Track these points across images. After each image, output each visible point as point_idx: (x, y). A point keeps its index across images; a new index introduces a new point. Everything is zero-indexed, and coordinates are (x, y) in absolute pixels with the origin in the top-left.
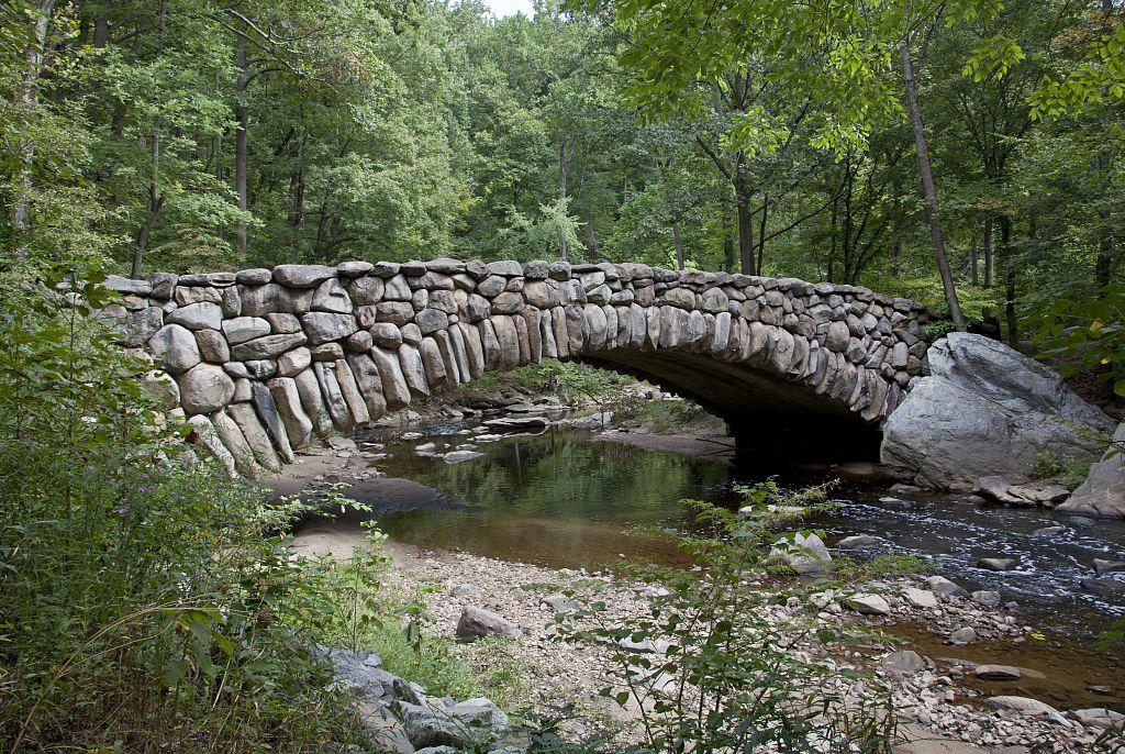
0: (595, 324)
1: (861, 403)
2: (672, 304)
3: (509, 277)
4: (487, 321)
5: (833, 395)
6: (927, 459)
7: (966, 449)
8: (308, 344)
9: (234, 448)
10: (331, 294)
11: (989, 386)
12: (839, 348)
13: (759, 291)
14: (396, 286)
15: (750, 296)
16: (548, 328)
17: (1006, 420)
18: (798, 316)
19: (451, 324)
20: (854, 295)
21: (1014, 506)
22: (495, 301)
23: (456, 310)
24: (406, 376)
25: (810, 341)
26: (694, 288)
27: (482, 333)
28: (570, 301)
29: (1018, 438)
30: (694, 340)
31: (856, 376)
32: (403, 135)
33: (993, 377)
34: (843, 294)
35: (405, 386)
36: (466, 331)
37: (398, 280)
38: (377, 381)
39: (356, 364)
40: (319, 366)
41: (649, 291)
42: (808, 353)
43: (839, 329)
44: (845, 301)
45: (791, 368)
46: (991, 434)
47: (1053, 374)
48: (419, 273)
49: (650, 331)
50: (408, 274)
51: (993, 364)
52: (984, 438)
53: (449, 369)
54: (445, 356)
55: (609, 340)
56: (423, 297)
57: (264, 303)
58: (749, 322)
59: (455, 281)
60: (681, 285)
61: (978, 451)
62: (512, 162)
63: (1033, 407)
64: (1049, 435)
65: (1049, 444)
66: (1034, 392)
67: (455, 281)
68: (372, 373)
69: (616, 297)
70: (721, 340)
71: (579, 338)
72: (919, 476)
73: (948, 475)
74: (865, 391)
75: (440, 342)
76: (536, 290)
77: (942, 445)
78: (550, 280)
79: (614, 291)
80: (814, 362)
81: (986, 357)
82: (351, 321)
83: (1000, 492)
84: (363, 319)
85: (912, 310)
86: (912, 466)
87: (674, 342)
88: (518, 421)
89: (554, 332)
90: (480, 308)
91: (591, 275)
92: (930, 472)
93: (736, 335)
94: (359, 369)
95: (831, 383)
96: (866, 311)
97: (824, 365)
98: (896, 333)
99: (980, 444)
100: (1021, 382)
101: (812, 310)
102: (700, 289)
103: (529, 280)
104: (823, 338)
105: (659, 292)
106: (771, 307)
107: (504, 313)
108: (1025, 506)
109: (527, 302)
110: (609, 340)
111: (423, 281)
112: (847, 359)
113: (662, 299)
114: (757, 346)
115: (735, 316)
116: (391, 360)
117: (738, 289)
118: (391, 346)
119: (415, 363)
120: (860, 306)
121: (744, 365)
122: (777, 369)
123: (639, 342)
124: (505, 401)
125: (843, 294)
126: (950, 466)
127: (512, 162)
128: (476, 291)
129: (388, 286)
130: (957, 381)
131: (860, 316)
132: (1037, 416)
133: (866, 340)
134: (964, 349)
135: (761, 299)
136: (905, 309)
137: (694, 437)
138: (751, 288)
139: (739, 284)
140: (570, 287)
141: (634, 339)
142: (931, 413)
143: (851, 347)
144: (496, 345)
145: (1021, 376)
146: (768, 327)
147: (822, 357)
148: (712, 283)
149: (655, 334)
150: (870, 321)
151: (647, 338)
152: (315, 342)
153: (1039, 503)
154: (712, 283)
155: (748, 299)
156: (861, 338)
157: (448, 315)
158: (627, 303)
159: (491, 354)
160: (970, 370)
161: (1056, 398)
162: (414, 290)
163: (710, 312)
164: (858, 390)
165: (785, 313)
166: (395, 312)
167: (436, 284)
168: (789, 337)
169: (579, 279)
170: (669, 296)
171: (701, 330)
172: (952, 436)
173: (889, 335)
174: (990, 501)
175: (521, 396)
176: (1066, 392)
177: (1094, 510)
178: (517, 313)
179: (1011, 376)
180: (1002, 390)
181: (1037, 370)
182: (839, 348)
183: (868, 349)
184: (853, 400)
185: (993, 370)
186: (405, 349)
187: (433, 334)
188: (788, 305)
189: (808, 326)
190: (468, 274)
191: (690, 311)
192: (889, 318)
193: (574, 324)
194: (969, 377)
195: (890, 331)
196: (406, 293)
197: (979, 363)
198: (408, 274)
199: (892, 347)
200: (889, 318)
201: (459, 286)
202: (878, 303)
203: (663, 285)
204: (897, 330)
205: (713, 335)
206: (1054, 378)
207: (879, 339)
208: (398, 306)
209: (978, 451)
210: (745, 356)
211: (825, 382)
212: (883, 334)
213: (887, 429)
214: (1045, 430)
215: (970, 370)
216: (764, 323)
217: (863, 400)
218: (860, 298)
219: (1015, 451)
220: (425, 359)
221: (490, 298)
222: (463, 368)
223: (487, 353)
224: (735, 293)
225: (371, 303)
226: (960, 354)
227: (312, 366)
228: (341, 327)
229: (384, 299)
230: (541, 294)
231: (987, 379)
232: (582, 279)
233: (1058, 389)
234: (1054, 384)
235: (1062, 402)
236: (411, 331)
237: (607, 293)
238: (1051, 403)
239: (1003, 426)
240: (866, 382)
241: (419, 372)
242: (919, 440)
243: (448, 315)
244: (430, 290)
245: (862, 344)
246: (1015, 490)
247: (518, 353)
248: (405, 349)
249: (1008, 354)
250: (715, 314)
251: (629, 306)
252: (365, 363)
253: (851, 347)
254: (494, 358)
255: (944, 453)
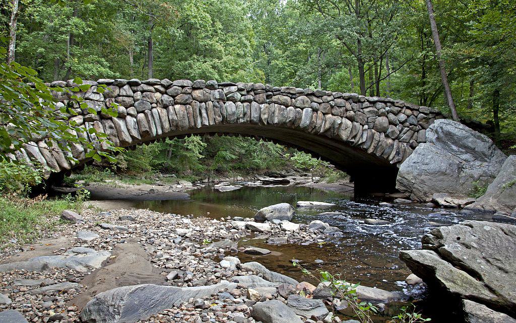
0: (229, 109)
1: (395, 160)
2: (275, 103)
3: (183, 87)
4: (170, 107)
6: (415, 185)
8: (82, 114)
10: (93, 93)
11: (454, 147)
12: (383, 130)
13: (329, 98)
14: (125, 90)
15: (324, 101)
16: (203, 111)
17: (458, 165)
18: (355, 112)
19: (152, 108)
20: (393, 103)
21: (446, 207)
22: (176, 98)
23: (155, 101)
24: (128, 130)
26: (291, 96)
27: (168, 112)
28: (216, 99)
29: (464, 175)
30: (288, 121)
31: (392, 145)
32: (219, 47)
33: (456, 142)
34: (385, 103)
36: (160, 111)
37: (126, 87)
38: (114, 131)
39: (104, 124)
40: (86, 123)
41: (262, 96)
43: (382, 120)
44: (387, 106)
47: (487, 140)
48: (137, 84)
49: (262, 115)
50: (131, 84)
52: (444, 174)
53: (150, 128)
54: (148, 122)
55: (238, 119)
56: (138, 95)
57: (62, 95)
58: (324, 114)
59: (155, 88)
60: (282, 93)
62: (290, 63)
63: (476, 159)
64: (481, 173)
67: (155, 88)
69: (243, 98)
70: (305, 121)
71: (219, 116)
72: (412, 195)
73: (425, 194)
74: (398, 153)
75: (146, 115)
76: (197, 93)
77: (423, 177)
78: (205, 89)
79: (242, 95)
80: (365, 136)
82: (102, 105)
83: (441, 201)
84: (108, 104)
85: (430, 113)
86: (409, 190)
87: (276, 121)
89: (207, 113)
90: (166, 101)
91: (229, 87)
92: (417, 192)
93: (314, 120)
95: (376, 148)
96: (400, 111)
97: (372, 137)
98: (420, 125)
99: (442, 177)
100: (470, 144)
101: (364, 110)
102: (294, 96)
103: (194, 89)
104: (372, 125)
105: (268, 97)
106: (338, 107)
107: (181, 104)
108: (452, 207)
109: (194, 99)
110: (238, 119)
111: (139, 88)
113: (270, 100)
114: (327, 126)
115: (315, 110)
116: (121, 123)
117: (318, 97)
118: (122, 116)
119: (133, 124)
120: (395, 109)
122: (342, 139)
123: (255, 120)
124: (286, 174)
125: (385, 103)
126: (426, 189)
127: (290, 63)
128: (166, 93)
129: (121, 90)
130: (439, 145)
131: (396, 114)
132: (478, 163)
133: (399, 127)
134: (441, 128)
135: (331, 102)
136: (426, 112)
137: (339, 183)
138: (325, 97)
139: (317, 94)
140: (216, 94)
141: (252, 119)
142: (419, 161)
144: (175, 118)
146: (335, 117)
147: (370, 133)
148: (301, 93)
149: (264, 117)
150: (402, 117)
151: (260, 120)
152: (85, 113)
153: (459, 205)
154: (301, 93)
155: (323, 102)
156: (396, 125)
157: (151, 104)
158: (250, 101)
160: (445, 139)
161: (488, 152)
162: (134, 92)
163: (299, 107)
164: (394, 153)
165: (347, 110)
166: (124, 101)
167: (145, 89)
168: (349, 122)
169: (222, 89)
170: (274, 98)
171: (292, 116)
174: (437, 205)
175: (295, 172)
177: (482, 209)
178: (187, 104)
179: (465, 141)
181: (479, 138)
182: (383, 130)
183: (400, 132)
184: (391, 157)
186: (128, 118)
187: (143, 112)
188: (348, 106)
189: (361, 117)
190: (162, 85)
191: (287, 106)
192: (416, 117)
193: (217, 110)
194: (444, 143)
195: (415, 123)
196: (131, 93)
197: (449, 134)
198: (131, 84)
200: (416, 117)
201: (157, 90)
202: (408, 108)
203: (271, 93)
205: (300, 119)
207: (408, 127)
208: (126, 99)
210: (322, 131)
211: (372, 147)
212: (411, 125)
213: (402, 168)
216: (333, 114)
217: (397, 158)
218: (396, 105)
219: (461, 181)
220: (138, 123)
221: (174, 97)
223: (171, 121)
224: (315, 99)
225: (112, 97)
226: (440, 130)
227: (84, 123)
228: (97, 107)
229: (119, 95)
230: (199, 95)
231: (453, 143)
232: (224, 89)
233: (489, 148)
234: (488, 145)
235: (492, 155)
236: (132, 110)
237: (238, 96)
238: (485, 155)
239: (455, 167)
240: (398, 148)
242: (411, 175)
243: (151, 104)
244: (142, 92)
245: (397, 129)
246: (449, 199)
247: (188, 122)
248: (128, 118)
249: (464, 130)
250: (302, 109)
251: (250, 103)
252: (108, 123)
253: (390, 130)
254: (175, 124)
255: (423, 182)
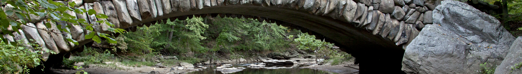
1: (401, 42)
5: (384, 36)
7: (441, 61)
9: (44, 38)
11: (461, 29)
17: (465, 46)
24: (129, 11)
25: (368, 7)
29: (471, 56)
31: (398, 27)
35: (127, 15)
38: (114, 13)
39: (104, 5)
42: (366, 12)
45: (355, 19)
46: (455, 53)
51: (463, 16)
52: (451, 55)
53: (151, 9)
61: (447, 62)
63: (484, 40)
64: (489, 54)
65: (489, 60)
66: (484, 31)
68: (111, 9)
74: (404, 35)
77: (429, 59)
81: (459, 12)
88: (279, 61)
94: (105, 7)
95: (381, 29)
98: (427, 6)
99: (448, 59)
100: (477, 26)
104: (377, 6)
112: (393, 18)
119: (133, 5)
121: (328, 17)
124: (290, 56)
130: (446, 27)
133: (405, 8)
134: (448, 9)
137: (344, 65)
142: (425, 43)
143: (395, 11)
145: (477, 23)
156: (402, 6)
159: (174, 3)
160: (451, 20)
161: (496, 34)
164: (399, 34)
172: (434, 55)
173: (422, 7)
176: (502, 31)
179: (472, 22)
180: (468, 31)
181: (486, 19)
185: (463, 20)
194: (451, 24)
195: (422, 4)
197: (456, 16)
199: (424, 13)
204: (427, 4)
206: (496, 23)
207: (414, 8)
209: (447, 62)
211: (377, 28)
212: (417, 6)
214: (487, 51)
215: (451, 20)
217: (403, 39)
219: (468, 63)
222: (158, 9)
226: (446, 11)
231: (460, 25)
233: (497, 29)
234: (495, 26)
235: (499, 36)
239: (462, 49)
240: (404, 29)
241: (135, 10)
242: (418, 57)
245: (403, 10)
249: (471, 11)
253: (395, 11)
254: (176, 5)
255: (429, 64)
